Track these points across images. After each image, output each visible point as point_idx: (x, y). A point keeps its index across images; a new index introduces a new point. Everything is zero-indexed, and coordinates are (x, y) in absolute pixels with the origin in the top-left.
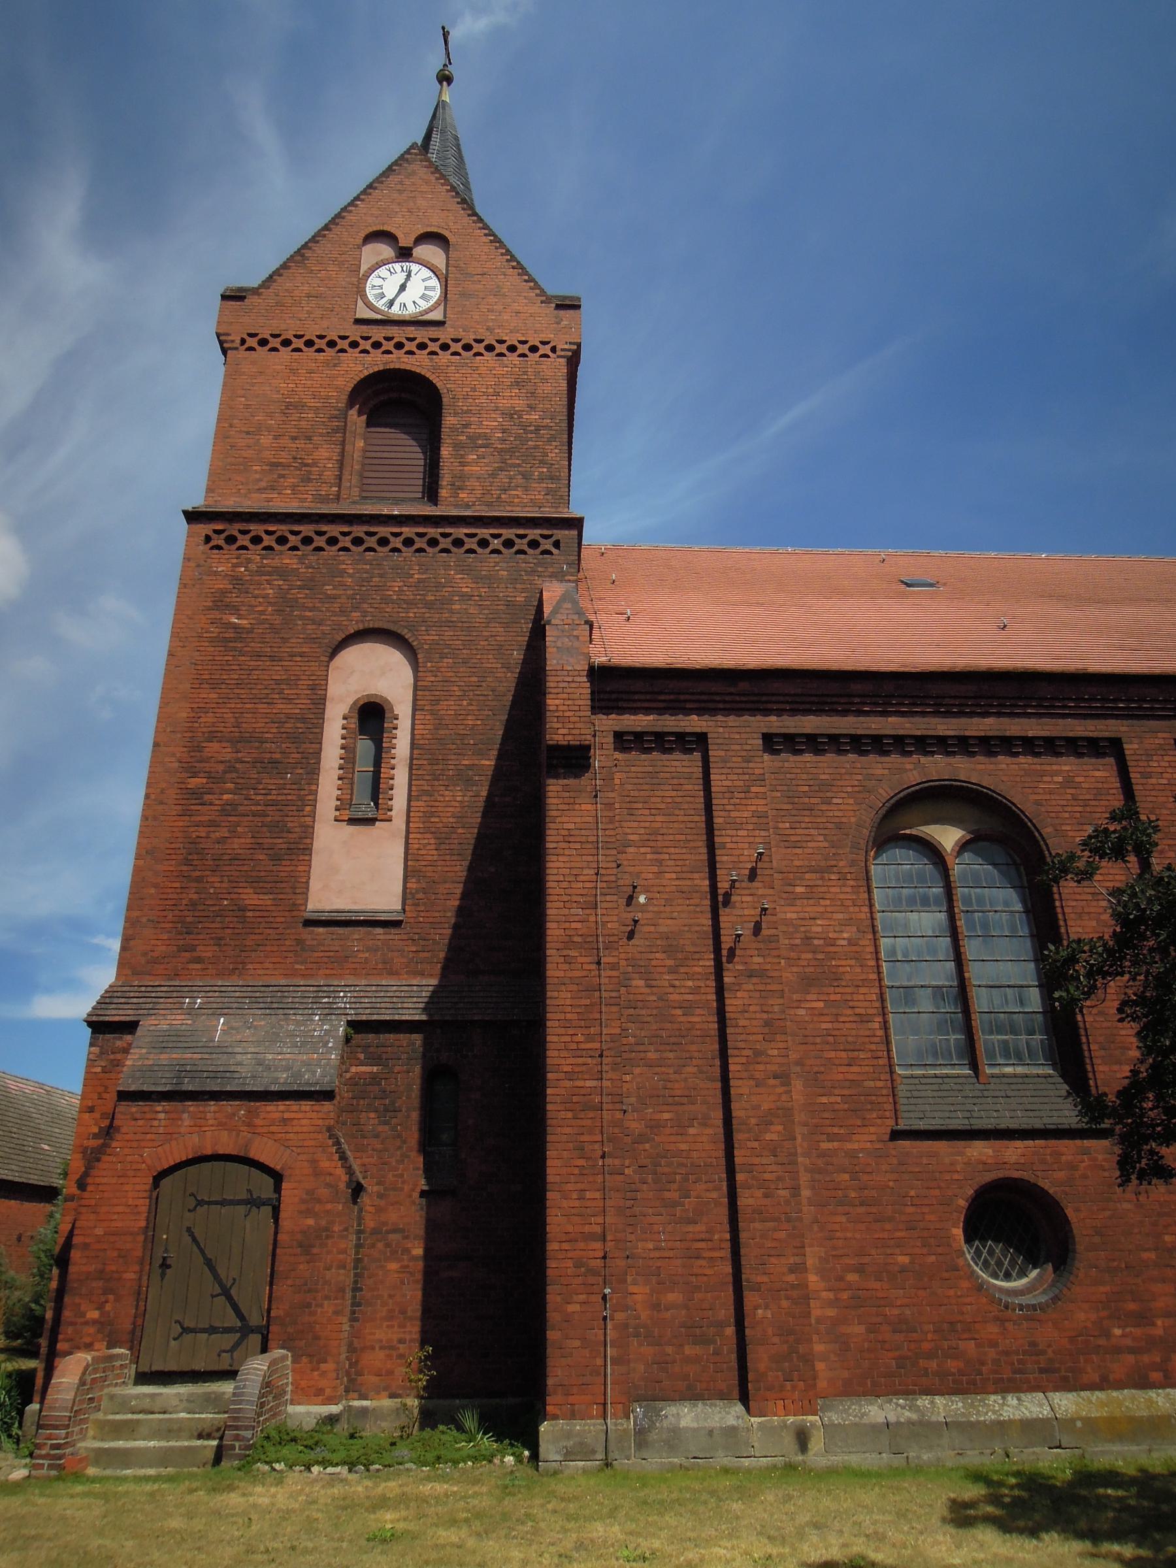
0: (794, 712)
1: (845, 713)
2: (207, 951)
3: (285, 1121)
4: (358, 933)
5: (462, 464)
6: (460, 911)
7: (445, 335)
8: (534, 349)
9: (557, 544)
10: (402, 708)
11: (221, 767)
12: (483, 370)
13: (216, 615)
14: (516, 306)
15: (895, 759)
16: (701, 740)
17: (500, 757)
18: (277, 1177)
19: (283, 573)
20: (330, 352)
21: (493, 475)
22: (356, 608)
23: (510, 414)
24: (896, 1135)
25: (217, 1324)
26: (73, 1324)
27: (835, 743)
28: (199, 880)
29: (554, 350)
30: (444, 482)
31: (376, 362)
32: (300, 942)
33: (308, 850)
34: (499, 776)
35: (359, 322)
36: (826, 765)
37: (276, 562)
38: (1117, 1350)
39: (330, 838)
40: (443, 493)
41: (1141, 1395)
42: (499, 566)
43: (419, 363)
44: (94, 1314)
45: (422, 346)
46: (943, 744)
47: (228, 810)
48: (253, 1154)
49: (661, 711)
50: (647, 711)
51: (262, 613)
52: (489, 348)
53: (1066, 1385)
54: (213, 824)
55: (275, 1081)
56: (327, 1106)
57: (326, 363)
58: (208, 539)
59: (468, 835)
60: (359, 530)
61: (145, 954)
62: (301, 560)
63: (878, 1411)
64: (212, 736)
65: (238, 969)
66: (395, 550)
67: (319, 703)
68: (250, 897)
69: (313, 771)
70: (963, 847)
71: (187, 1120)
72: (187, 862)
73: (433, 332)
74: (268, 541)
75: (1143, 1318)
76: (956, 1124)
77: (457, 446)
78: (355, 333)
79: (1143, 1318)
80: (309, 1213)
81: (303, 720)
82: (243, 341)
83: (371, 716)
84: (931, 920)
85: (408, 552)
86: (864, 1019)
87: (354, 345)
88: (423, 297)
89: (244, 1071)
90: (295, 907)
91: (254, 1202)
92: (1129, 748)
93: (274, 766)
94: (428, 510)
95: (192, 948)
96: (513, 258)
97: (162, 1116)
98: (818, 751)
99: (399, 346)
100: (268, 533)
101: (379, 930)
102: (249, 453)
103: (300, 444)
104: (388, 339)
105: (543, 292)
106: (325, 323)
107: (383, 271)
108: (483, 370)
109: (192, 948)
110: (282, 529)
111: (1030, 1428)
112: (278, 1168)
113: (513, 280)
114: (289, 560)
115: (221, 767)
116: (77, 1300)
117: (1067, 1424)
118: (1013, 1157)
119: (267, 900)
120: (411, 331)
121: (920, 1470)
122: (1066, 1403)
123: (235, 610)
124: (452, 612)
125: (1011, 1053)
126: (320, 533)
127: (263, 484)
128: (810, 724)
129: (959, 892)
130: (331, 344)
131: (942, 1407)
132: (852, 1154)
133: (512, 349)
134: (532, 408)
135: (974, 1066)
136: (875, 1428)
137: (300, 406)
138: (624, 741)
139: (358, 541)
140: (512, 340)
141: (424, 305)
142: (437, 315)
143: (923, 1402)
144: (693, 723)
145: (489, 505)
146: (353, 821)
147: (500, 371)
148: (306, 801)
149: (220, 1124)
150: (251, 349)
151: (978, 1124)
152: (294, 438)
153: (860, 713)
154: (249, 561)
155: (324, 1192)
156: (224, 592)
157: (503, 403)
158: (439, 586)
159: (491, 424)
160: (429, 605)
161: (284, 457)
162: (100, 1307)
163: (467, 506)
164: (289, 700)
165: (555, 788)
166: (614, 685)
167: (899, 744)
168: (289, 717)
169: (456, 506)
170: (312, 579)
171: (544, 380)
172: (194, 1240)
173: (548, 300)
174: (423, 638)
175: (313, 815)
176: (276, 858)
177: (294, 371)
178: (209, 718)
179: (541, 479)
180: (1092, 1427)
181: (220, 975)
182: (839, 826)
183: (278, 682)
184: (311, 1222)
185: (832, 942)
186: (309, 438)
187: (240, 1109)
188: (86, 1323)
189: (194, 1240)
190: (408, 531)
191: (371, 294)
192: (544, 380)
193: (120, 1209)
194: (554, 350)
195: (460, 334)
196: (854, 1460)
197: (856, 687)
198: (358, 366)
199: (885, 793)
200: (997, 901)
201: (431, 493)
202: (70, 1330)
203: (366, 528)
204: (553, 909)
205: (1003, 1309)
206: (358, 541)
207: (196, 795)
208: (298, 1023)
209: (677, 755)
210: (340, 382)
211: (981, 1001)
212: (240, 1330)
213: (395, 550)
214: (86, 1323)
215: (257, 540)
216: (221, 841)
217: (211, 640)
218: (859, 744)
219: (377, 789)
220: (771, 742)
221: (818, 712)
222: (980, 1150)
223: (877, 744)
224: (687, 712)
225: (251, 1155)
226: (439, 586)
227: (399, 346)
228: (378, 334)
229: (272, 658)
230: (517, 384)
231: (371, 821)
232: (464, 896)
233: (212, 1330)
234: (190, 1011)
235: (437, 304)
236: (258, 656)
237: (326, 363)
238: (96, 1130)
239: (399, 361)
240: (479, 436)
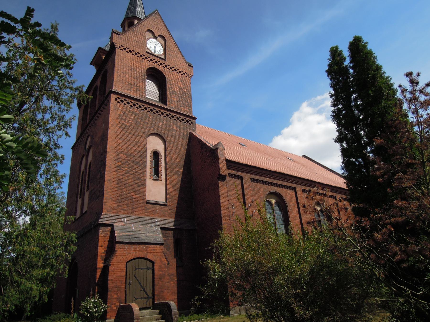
0: (255, 174)
2: (125, 208)
3: (154, 250)
4: (158, 207)
6: (178, 203)
9: (192, 122)
10: (162, 154)
11: (124, 161)
13: (119, 120)
16: (241, 177)
18: (153, 263)
22: (152, 127)
23: (181, 88)
25: (143, 297)
26: (110, 299)
28: (122, 189)
31: (151, 65)
32: (145, 207)
33: (145, 185)
34: (184, 174)
36: (259, 185)
39: (149, 183)
40: (168, 103)
44: (115, 296)
47: (127, 172)
48: (148, 257)
49: (235, 170)
50: (233, 170)
51: (131, 123)
54: (123, 175)
55: (151, 240)
56: (162, 247)
57: (140, 61)
59: (178, 186)
61: (110, 207)
64: (121, 152)
65: (132, 213)
71: (132, 249)
72: (118, 184)
77: (170, 92)
80: (160, 271)
82: (120, 47)
88: (160, 51)
89: (144, 237)
91: (148, 269)
92: (297, 189)
93: (137, 163)
95: (121, 206)
96: (179, 50)
97: (127, 248)
101: (162, 206)
102: (124, 78)
103: (135, 80)
109: (121, 206)
112: (153, 260)
113: (179, 55)
114: (136, 110)
115: (124, 161)
116: (111, 293)
119: (137, 196)
120: (155, 58)
123: (124, 120)
124: (172, 133)
127: (127, 88)
128: (280, 182)
134: (185, 88)
138: (231, 175)
144: (240, 174)
145: (177, 109)
148: (144, 173)
149: (140, 250)
152: (134, 78)
153: (264, 176)
155: (163, 266)
159: (177, 89)
160: (168, 130)
162: (117, 294)
163: (173, 108)
165: (220, 183)
166: (231, 164)
168: (139, 151)
172: (136, 278)
173: (187, 63)
176: (139, 186)
177: (133, 60)
178: (120, 148)
181: (128, 214)
184: (161, 273)
187: (144, 247)
188: (114, 299)
189: (136, 278)
193: (119, 270)
197: (264, 172)
202: (110, 300)
204: (222, 208)
207: (119, 167)
208: (150, 227)
209: (237, 180)
212: (147, 298)
214: (114, 299)
216: (126, 180)
219: (157, 172)
220: (253, 180)
221: (258, 175)
224: (239, 171)
225: (147, 257)
230: (181, 81)
231: (157, 180)
232: (178, 200)
233: (141, 298)
234: (124, 222)
237: (140, 61)
238: (103, 251)
239: (156, 66)
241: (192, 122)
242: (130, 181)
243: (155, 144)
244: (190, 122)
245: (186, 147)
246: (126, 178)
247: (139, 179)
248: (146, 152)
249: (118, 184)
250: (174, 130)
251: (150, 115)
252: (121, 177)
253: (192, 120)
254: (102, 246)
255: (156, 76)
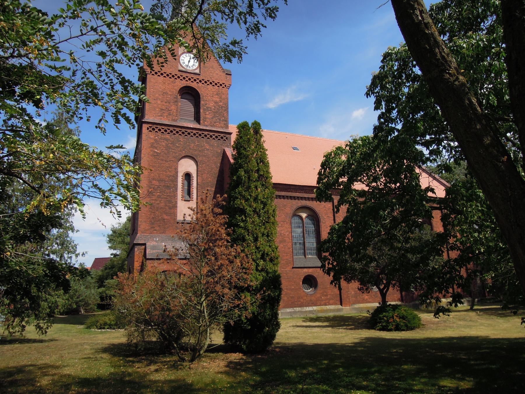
0: (281, 191)
1: (289, 192)
2: (157, 228)
5: (205, 115)
7: (201, 78)
8: (221, 85)
9: (227, 138)
10: (194, 175)
12: (209, 89)
13: (151, 149)
14: (217, 72)
15: (297, 201)
17: (215, 188)
19: (167, 140)
20: (173, 79)
21: (212, 118)
22: (184, 150)
23: (216, 103)
24: (293, 268)
27: (288, 197)
28: (154, 212)
29: (225, 86)
30: (201, 119)
31: (184, 83)
32: (176, 227)
35: (179, 71)
37: (165, 137)
38: (322, 300)
40: (201, 122)
41: (325, 307)
42: (215, 142)
43: (194, 85)
45: (195, 80)
46: (305, 199)
47: (159, 197)
52: (211, 83)
53: (315, 305)
54: (155, 200)
58: (148, 129)
60: (183, 130)
62: (171, 136)
63: (288, 310)
64: (154, 179)
65: (164, 232)
66: (192, 136)
67: (177, 173)
68: (165, 217)
69: (176, 189)
70: (306, 217)
72: (151, 208)
73: (197, 77)
74: (162, 131)
75: (326, 295)
76: (302, 266)
77: (204, 110)
78: (179, 74)
79: (326, 295)
81: (174, 177)
83: (188, 176)
84: (300, 230)
85: (195, 137)
86: (289, 248)
87: (179, 77)
90: (175, 219)
93: (168, 187)
94: (198, 126)
95: (154, 228)
98: (284, 199)
99: (190, 79)
100: (163, 129)
102: (155, 105)
103: (167, 104)
104: (187, 77)
105: (223, 69)
106: (171, 70)
107: (184, 55)
108: (209, 89)
109: (154, 228)
110: (166, 128)
111: (310, 312)
114: (168, 136)
117: (315, 311)
118: (310, 271)
120: (192, 76)
121: (294, 318)
122: (315, 308)
123: (156, 148)
125: (311, 254)
126: (175, 130)
129: (305, 225)
130: (173, 76)
131: (298, 309)
132: (286, 271)
133: (216, 84)
134: (221, 101)
135: (305, 256)
136: (288, 312)
137: (166, 93)
139: (183, 133)
140: (216, 82)
141: (195, 68)
142: (197, 71)
143: (295, 308)
146: (185, 200)
147: (213, 90)
148: (175, 196)
150: (153, 75)
151: (306, 266)
152: (166, 102)
154: (158, 135)
156: (153, 143)
157: (215, 99)
158: (202, 146)
159: (212, 104)
161: (164, 108)
164: (170, 172)
167: (298, 198)
168: (170, 176)
169: (204, 126)
170: (173, 142)
171: (223, 94)
174: (199, 159)
175: (177, 199)
177: (164, 83)
179: (223, 121)
180: (319, 311)
181: (160, 233)
182: (287, 213)
183: (167, 167)
185: (285, 235)
186: (169, 103)
190: (194, 132)
191: (181, 62)
192: (223, 94)
194: (225, 86)
195: (204, 78)
196: (285, 317)
197: (292, 187)
198: (181, 84)
199: (295, 207)
200: (310, 227)
201: (197, 119)
203: (185, 130)
205: (307, 294)
206: (183, 133)
210: (176, 88)
211: (307, 245)
213: (192, 136)
215: (160, 130)
216: (158, 204)
217: (151, 155)
218: (291, 198)
219: (189, 193)
222: (305, 270)
223: (294, 198)
226: (202, 146)
227: (190, 79)
228: (185, 75)
229: (166, 161)
234: (156, 241)
235: (197, 68)
236: (163, 160)
237: (172, 82)
240: (209, 107)
241: (227, 138)
242: (162, 205)
243: (187, 166)
244: (225, 138)
245: (219, 165)
246: (158, 202)
247: (170, 202)
248: (177, 176)
249: (151, 208)
250: (207, 149)
251: (181, 138)
252: (154, 202)
253: (227, 136)
254: (137, 261)
255: (190, 94)
